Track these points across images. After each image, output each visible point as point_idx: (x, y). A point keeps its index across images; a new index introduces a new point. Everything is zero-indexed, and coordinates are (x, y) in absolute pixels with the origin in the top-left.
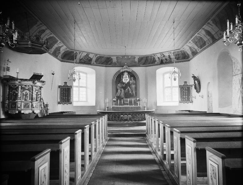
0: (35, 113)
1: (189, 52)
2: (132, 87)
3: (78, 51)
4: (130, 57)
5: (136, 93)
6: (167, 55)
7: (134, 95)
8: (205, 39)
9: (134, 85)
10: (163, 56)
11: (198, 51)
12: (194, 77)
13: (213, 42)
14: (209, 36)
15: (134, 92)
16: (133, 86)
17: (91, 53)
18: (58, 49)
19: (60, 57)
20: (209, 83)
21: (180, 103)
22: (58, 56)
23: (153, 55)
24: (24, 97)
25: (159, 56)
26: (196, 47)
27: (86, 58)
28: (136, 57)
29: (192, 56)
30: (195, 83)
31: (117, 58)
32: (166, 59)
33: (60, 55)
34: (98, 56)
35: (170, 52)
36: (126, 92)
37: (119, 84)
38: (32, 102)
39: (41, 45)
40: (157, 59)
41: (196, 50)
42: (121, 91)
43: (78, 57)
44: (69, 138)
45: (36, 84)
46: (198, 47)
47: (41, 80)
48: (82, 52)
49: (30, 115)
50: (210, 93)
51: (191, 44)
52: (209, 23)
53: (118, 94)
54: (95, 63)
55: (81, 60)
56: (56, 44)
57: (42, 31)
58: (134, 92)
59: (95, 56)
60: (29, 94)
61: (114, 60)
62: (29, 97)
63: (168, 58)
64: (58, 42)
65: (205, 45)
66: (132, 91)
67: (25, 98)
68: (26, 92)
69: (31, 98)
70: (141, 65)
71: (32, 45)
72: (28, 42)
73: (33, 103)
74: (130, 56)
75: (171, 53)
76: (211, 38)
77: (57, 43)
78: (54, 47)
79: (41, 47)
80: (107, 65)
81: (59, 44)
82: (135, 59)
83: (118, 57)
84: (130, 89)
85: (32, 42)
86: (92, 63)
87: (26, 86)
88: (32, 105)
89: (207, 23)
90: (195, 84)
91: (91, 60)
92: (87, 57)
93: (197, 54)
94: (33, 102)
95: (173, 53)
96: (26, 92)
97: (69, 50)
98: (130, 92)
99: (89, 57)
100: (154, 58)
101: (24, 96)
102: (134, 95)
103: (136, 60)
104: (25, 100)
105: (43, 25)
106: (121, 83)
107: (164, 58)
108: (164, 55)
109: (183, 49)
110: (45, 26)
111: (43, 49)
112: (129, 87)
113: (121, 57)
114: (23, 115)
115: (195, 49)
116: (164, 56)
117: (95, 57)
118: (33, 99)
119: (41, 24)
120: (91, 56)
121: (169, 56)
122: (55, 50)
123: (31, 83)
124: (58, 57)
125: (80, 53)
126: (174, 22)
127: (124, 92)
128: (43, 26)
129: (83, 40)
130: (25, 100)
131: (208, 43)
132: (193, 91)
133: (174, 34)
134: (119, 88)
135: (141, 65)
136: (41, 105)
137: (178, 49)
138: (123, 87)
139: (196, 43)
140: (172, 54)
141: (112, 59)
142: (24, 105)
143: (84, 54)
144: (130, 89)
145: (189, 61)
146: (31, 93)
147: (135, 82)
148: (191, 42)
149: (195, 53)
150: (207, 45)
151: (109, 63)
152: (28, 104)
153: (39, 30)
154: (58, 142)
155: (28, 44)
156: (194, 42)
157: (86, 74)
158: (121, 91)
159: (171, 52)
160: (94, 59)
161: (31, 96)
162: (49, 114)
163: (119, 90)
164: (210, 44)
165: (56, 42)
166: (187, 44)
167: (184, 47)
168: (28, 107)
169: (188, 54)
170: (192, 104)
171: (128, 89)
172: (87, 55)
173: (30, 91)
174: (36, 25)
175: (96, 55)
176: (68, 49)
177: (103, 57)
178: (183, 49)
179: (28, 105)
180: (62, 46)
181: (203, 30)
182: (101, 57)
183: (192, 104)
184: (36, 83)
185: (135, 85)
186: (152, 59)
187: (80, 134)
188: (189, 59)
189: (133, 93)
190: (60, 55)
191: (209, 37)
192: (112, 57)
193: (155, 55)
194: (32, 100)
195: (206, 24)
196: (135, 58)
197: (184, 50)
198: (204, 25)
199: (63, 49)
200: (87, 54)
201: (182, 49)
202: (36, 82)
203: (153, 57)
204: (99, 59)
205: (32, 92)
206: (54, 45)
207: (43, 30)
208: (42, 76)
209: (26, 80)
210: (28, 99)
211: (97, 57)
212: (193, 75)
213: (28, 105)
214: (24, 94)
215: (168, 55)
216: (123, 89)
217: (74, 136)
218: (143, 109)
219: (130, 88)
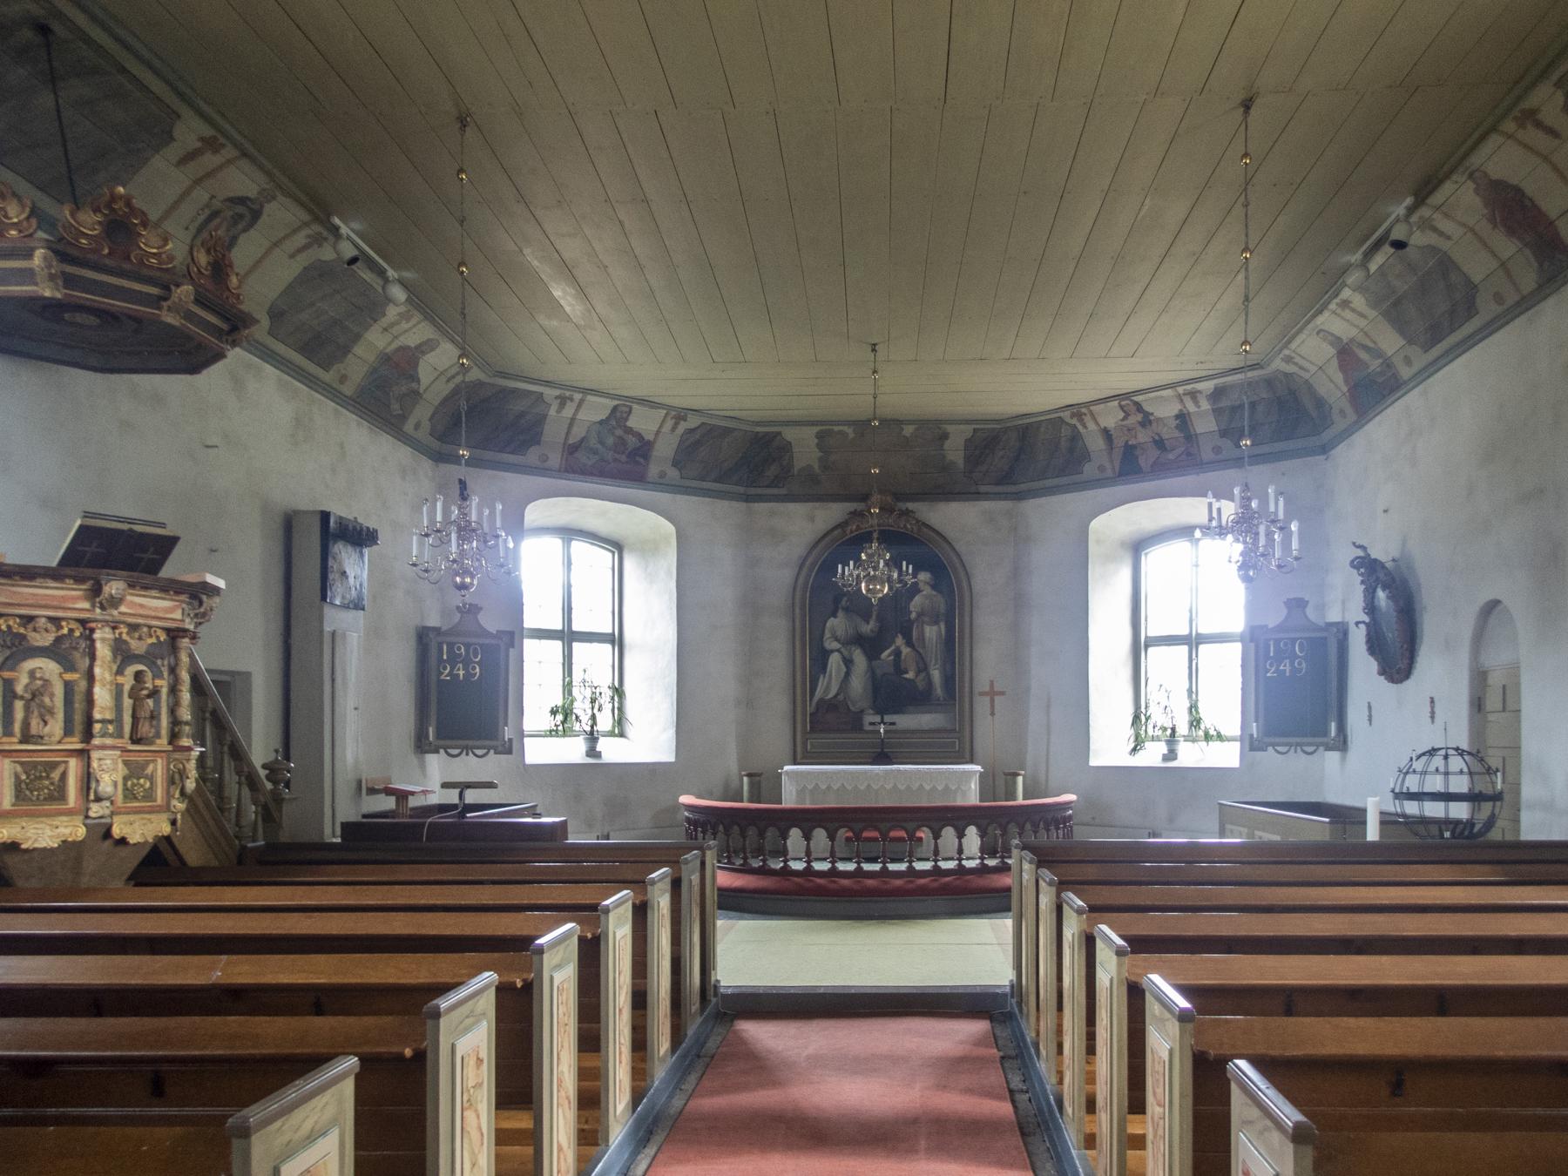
0: (123, 841)
1: (1333, 386)
2: (922, 634)
3: (548, 383)
4: (908, 430)
5: (949, 680)
6: (1165, 409)
7: (939, 690)
8: (1476, 266)
9: (936, 623)
10: (1140, 417)
11: (1405, 372)
12: (1369, 568)
13: (1540, 287)
14: (1511, 232)
15: (936, 675)
16: (932, 633)
17: (642, 401)
18: (402, 364)
19: (426, 425)
20: (1492, 606)
21: (1252, 749)
22: (403, 418)
23: (1066, 415)
24: (19, 714)
25: (1110, 417)
26: (1390, 342)
27: (610, 441)
28: (950, 428)
29: (1349, 410)
30: (1371, 607)
31: (820, 436)
32: (1160, 443)
33: (421, 414)
34: (693, 422)
35: (1184, 388)
36: (879, 672)
37: (834, 615)
38: (83, 754)
39: (150, 281)
40: (1095, 444)
41: (1388, 364)
42: (848, 662)
43: (553, 431)
44: (489, 977)
45: (123, 609)
46: (1410, 342)
47: (167, 572)
48: (578, 396)
49: (78, 860)
50: (1495, 680)
51: (1350, 317)
52: (1345, 304)
53: (828, 686)
54: (673, 473)
55: (572, 449)
56: (377, 327)
57: (240, 209)
58: (936, 675)
59: (669, 423)
60: (59, 691)
61: (805, 449)
62: (60, 715)
63: (1169, 432)
64: (392, 312)
65: (1471, 310)
66: (923, 668)
67: (26, 725)
68: (32, 674)
69: (78, 718)
70: (983, 489)
71: (69, 281)
72: (29, 255)
73: (95, 764)
74: (910, 422)
75: (1193, 395)
76: (1527, 252)
77: (384, 322)
78: (359, 349)
79: (157, 301)
80: (752, 491)
81: (397, 327)
82: (947, 444)
83: (826, 431)
84: (905, 650)
85: (63, 257)
86: (653, 471)
87: (30, 619)
88: (88, 779)
89: (1516, 112)
90: (1374, 619)
91: (646, 457)
92: (619, 432)
93: (1393, 390)
94: (95, 755)
95: (1217, 394)
96: (32, 674)
97: (482, 377)
98: (910, 675)
99: (629, 431)
100: (1076, 437)
101: (19, 706)
102: (939, 690)
103: (954, 451)
104: (26, 738)
105: (229, 152)
106: (846, 610)
107: (1143, 437)
108: (1147, 415)
109: (1288, 360)
110: (245, 164)
111: (170, 319)
112: (900, 641)
113: (849, 430)
114: (11, 860)
115: (1377, 353)
116: (1147, 420)
117: (674, 429)
118: (97, 727)
119: (211, 145)
120: (643, 422)
121: (1183, 419)
122: (374, 370)
123: (71, 599)
124: (409, 427)
125: (563, 401)
126: (1247, 105)
127: (871, 671)
128: (229, 162)
129: (594, 313)
130: (26, 738)
131: (1498, 298)
132: (1363, 668)
133: (1246, 205)
134: (835, 645)
135: (983, 489)
136: (183, 774)
137: (1253, 367)
138: (859, 640)
139: (1396, 304)
140: (1205, 405)
141: (786, 448)
142: (17, 776)
143: (595, 411)
144: (905, 650)
145: (1324, 449)
146: (83, 685)
147: (941, 603)
148: (1358, 301)
149: (1373, 389)
150: (1487, 309)
151: (772, 471)
152: (54, 765)
153: (201, 195)
154: (417, 1003)
155: (28, 276)
156: (1374, 304)
157: (617, 546)
158: (848, 662)
159: (1200, 386)
160: (665, 448)
161: (79, 706)
162: (346, 827)
163: (835, 660)
164: (1510, 302)
165: (372, 308)
166: (1320, 320)
167: (1293, 345)
168: (59, 794)
169: (1320, 403)
170: (1343, 759)
171: (897, 653)
172: (619, 416)
173: (69, 666)
174: (173, 151)
175: (680, 415)
176: (475, 374)
177: (727, 431)
178: (1288, 360)
179: (56, 775)
180: (426, 347)
181: (1471, 185)
182: (713, 428)
183: (1343, 759)
184: (115, 602)
185: (942, 626)
186: (1064, 444)
187: (666, 885)
188: (1327, 436)
189: (930, 683)
190: (421, 414)
191: (1507, 247)
192: (790, 434)
193: (1079, 416)
194: (88, 735)
195: (1509, 126)
196: (945, 436)
197: (1290, 369)
198: (1483, 138)
199: (440, 364)
200: (615, 408)
201: (1278, 364)
202: (114, 587)
203: (1065, 432)
204: (698, 443)
205: (91, 668)
206: (357, 337)
207: (242, 201)
208: (172, 541)
209: (28, 574)
210: (56, 727)
211: (692, 431)
212: (1360, 553)
213: (56, 775)
214: (19, 689)
215: (1174, 409)
216: (865, 652)
217: (645, 892)
218: (1001, 789)
219: (909, 643)
